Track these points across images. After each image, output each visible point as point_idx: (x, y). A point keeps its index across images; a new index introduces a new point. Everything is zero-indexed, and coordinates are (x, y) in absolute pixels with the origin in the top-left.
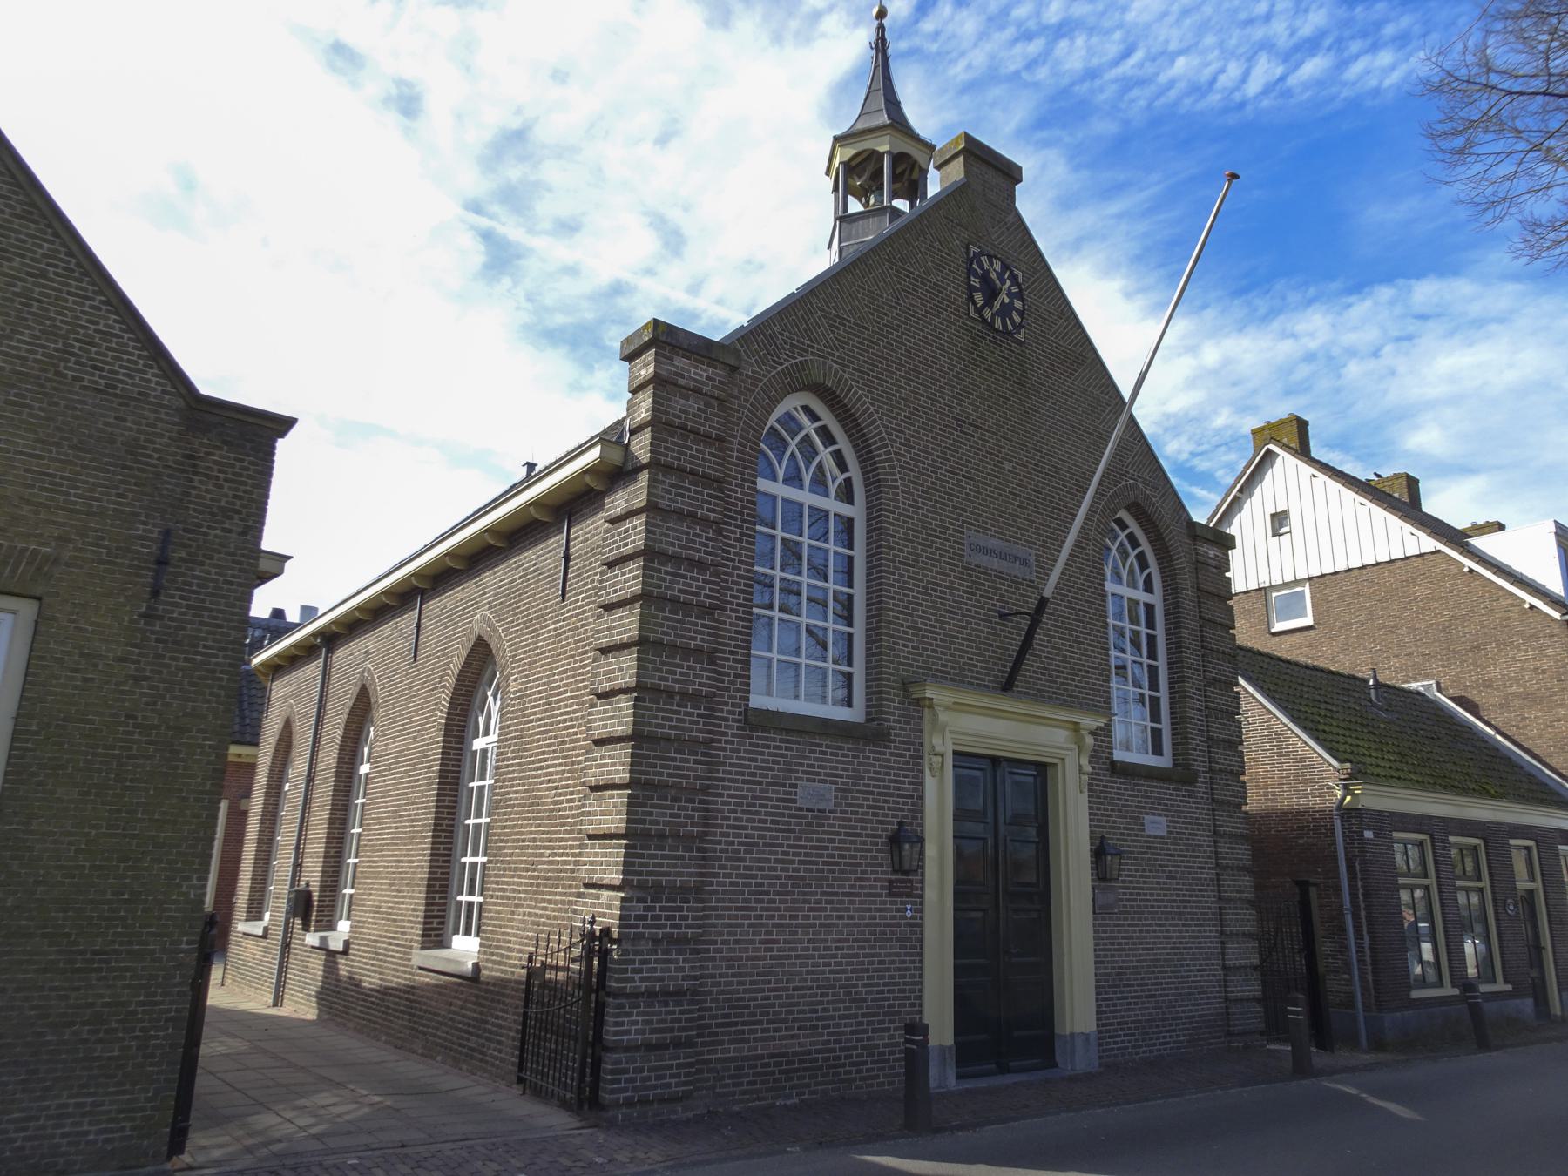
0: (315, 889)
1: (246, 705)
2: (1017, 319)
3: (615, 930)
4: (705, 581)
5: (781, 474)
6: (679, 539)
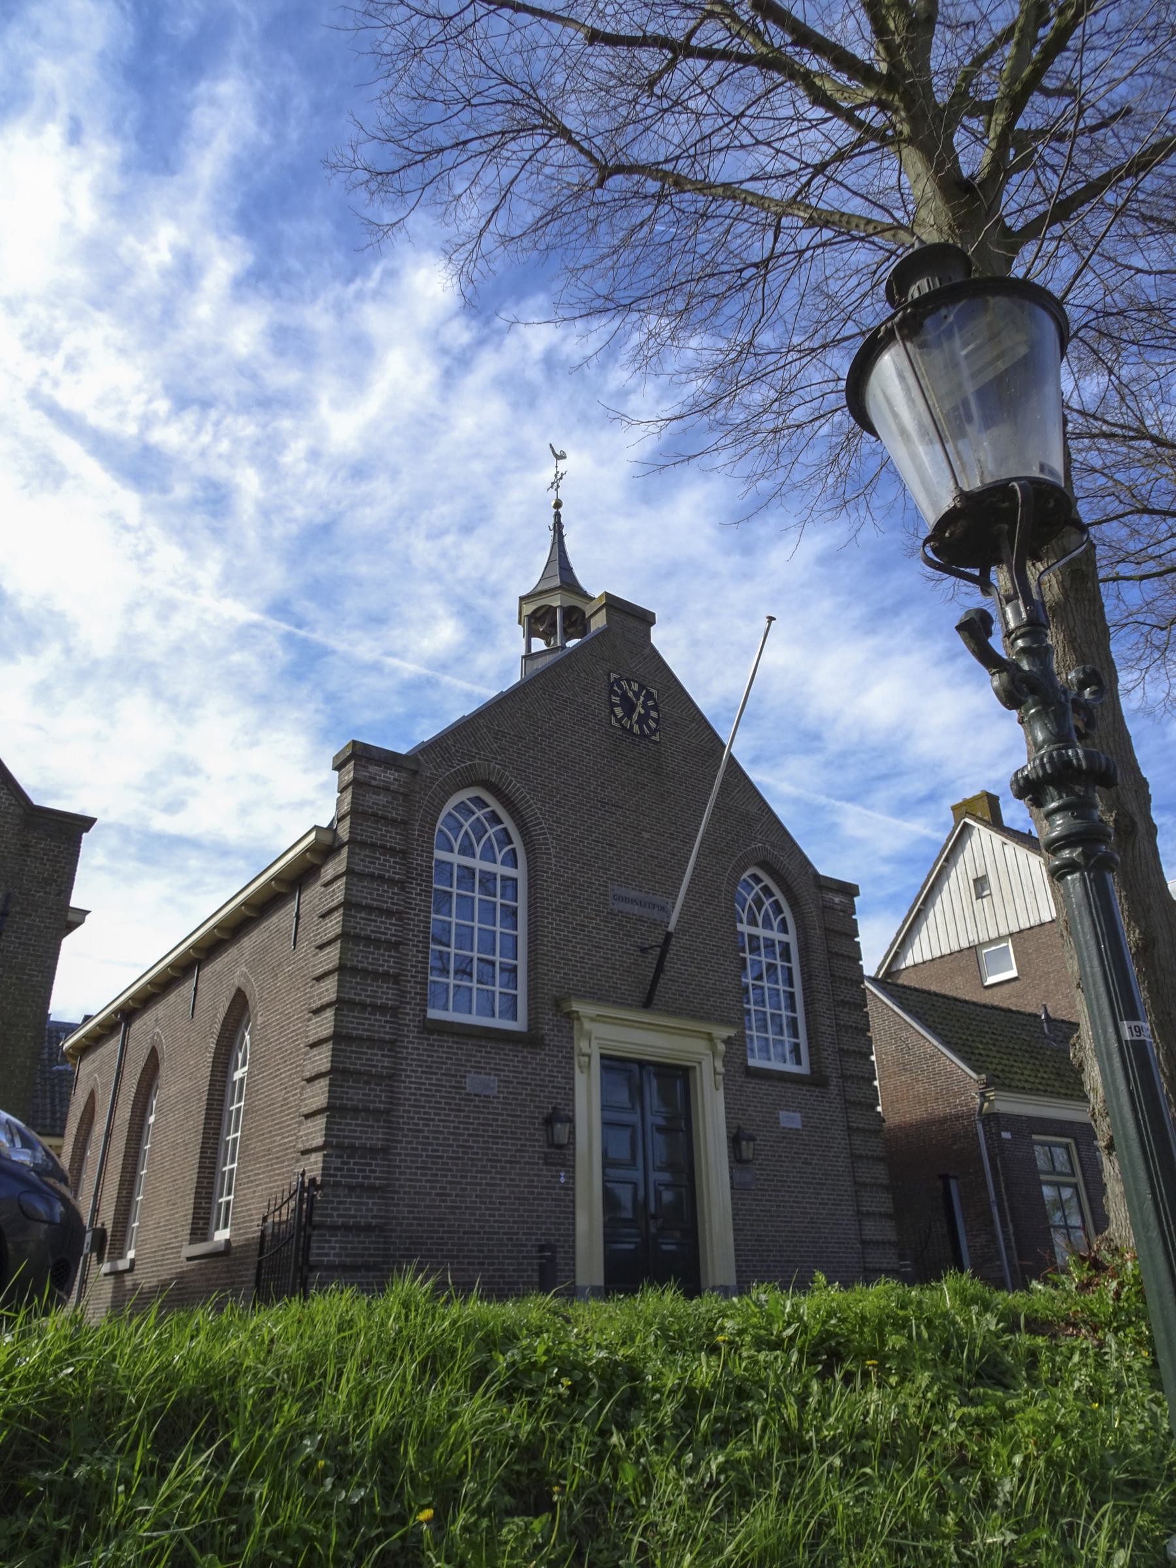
0: (109, 1227)
1: (57, 1101)
2: (653, 725)
3: (319, 1179)
4: (391, 924)
5: (456, 847)
6: (371, 894)
